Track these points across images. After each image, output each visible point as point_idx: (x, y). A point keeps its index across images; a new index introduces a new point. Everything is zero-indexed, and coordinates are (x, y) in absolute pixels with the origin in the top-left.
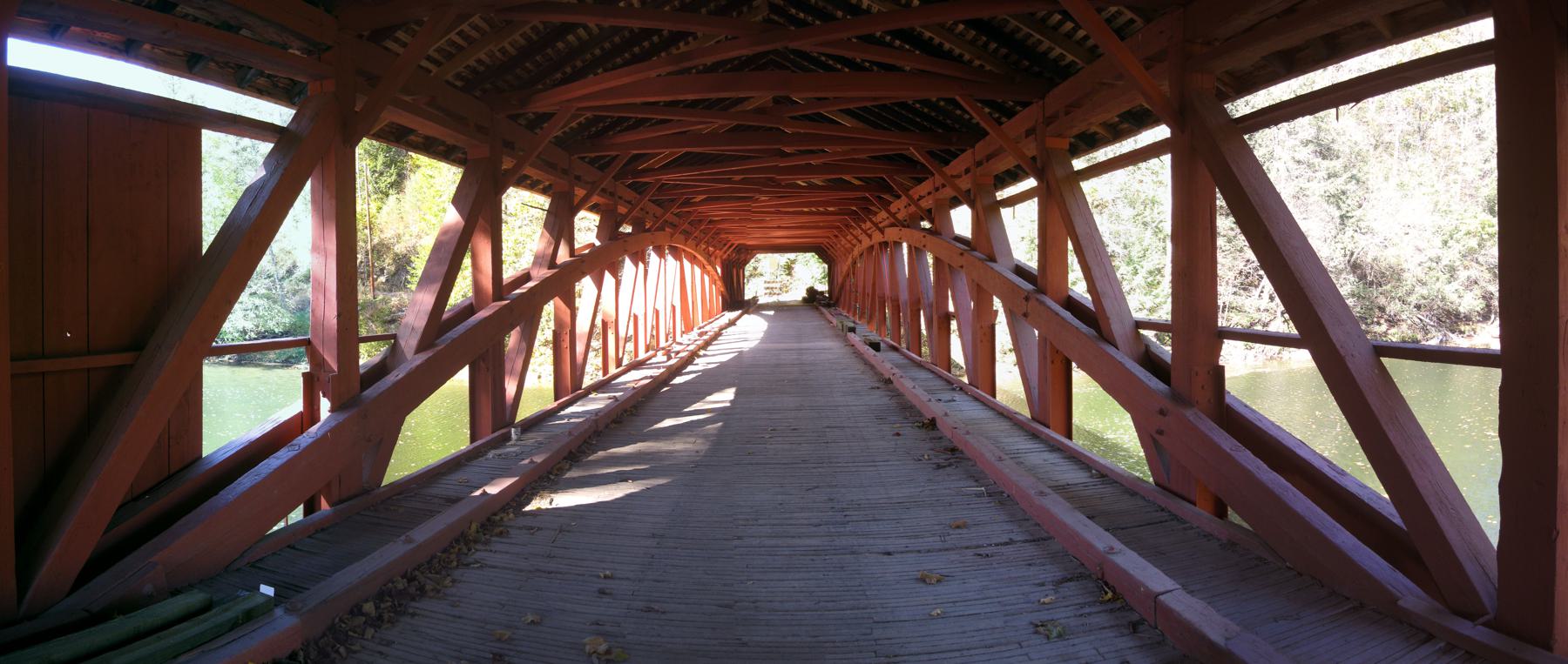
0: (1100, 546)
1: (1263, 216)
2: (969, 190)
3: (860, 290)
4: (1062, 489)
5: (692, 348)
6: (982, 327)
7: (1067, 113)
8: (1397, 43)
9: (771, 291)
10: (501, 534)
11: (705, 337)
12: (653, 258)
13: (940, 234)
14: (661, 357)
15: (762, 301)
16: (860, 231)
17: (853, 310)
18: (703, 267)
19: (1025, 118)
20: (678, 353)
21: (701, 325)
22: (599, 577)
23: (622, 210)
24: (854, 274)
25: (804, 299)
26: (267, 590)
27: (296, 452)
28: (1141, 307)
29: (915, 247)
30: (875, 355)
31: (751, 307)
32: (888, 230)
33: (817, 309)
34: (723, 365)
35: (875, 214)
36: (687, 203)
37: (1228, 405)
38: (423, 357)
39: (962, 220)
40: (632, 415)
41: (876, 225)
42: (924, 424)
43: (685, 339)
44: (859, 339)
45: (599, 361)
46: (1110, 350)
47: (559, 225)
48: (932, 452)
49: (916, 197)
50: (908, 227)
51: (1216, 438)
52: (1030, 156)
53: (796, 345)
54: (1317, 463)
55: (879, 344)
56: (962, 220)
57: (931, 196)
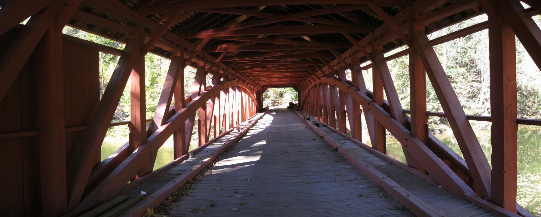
0: (380, 177)
1: (435, 75)
2: (337, 70)
3: (312, 103)
4: (378, 167)
5: (247, 127)
6: (356, 115)
7: (381, 38)
8: (482, 14)
9: (274, 104)
10: (199, 181)
11: (252, 123)
12: (231, 90)
13: (341, 80)
14: (235, 130)
15: (270, 108)
16: (311, 79)
17: (309, 111)
18: (249, 95)
19: (368, 39)
20: (242, 128)
21: (249, 118)
22: (234, 189)
23: (221, 72)
24: (309, 96)
25: (288, 107)
26: (143, 193)
27: (133, 158)
28: (433, 108)
29: (332, 86)
30: (317, 128)
31: (266, 111)
32: (322, 78)
33: (294, 111)
34: (259, 133)
35: (317, 71)
36: (244, 69)
37: (430, 138)
38: (164, 127)
39: (349, 75)
40: (231, 149)
41: (317, 76)
42: (333, 150)
43: (244, 123)
44: (311, 122)
45: (213, 134)
46: (394, 120)
47: (200, 79)
48: (335, 158)
49: (332, 65)
50: (330, 77)
51: (422, 148)
52: (369, 53)
53: (285, 126)
54: (453, 155)
55: (319, 124)
56: (349, 75)
57: (337, 65)
